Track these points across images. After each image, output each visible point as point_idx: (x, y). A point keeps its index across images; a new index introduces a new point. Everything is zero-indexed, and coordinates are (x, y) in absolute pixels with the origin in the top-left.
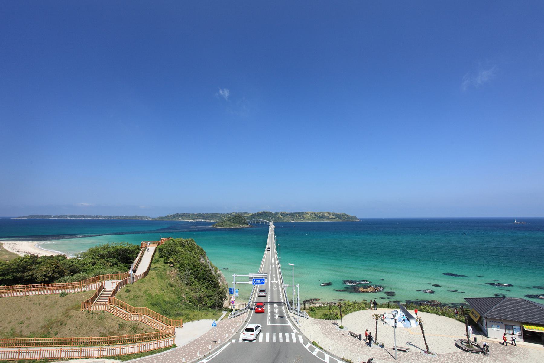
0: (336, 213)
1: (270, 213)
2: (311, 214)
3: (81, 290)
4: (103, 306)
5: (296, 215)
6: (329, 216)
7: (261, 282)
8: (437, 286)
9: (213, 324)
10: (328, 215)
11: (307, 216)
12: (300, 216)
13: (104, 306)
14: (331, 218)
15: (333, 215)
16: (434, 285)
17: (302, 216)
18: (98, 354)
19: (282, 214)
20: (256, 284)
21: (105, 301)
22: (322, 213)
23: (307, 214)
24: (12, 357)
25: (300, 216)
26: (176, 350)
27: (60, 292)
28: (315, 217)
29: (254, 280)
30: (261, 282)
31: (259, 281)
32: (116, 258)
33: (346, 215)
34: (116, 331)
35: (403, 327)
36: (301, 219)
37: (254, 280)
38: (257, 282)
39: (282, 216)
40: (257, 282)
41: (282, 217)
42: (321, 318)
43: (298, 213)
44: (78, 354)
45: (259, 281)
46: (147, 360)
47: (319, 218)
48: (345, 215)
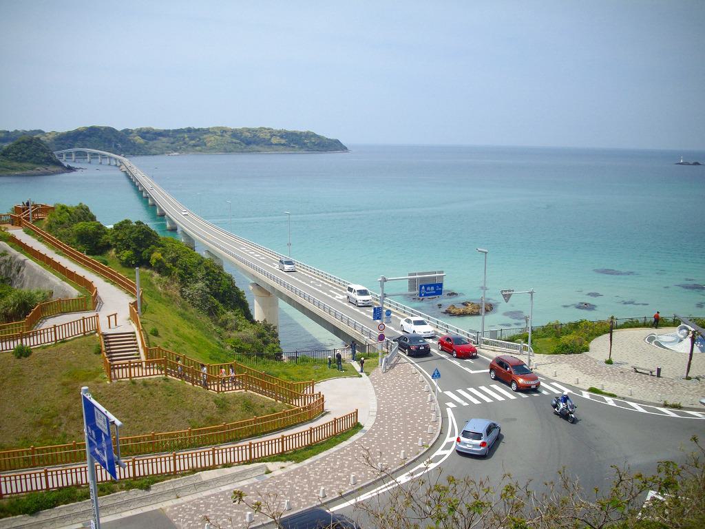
0: (290, 129)
1: (112, 130)
2: (224, 134)
3: (22, 341)
4: (124, 370)
5: (182, 135)
6: (270, 139)
7: (436, 291)
8: (595, 295)
9: (434, 374)
10: (268, 136)
11: (213, 139)
12: (193, 140)
13: (128, 370)
14: (276, 144)
15: (282, 137)
16: (589, 294)
17: (200, 139)
18: (245, 456)
19: (144, 133)
20: (426, 295)
21: (128, 359)
22: (253, 131)
23: (212, 133)
24: (79, 480)
25: (192, 139)
26: (368, 434)
27: (14, 345)
28: (234, 140)
29: (423, 288)
30: (436, 291)
31: (432, 288)
32: (113, 252)
33: (314, 135)
34: (216, 416)
35: (700, 352)
36: (198, 148)
37: (423, 288)
38: (428, 291)
39: (143, 138)
40: (428, 291)
41: (142, 141)
42: (555, 353)
43: (189, 130)
44: (208, 461)
45: (432, 288)
46: (175, 508)
47: (244, 145)
48: (312, 136)
